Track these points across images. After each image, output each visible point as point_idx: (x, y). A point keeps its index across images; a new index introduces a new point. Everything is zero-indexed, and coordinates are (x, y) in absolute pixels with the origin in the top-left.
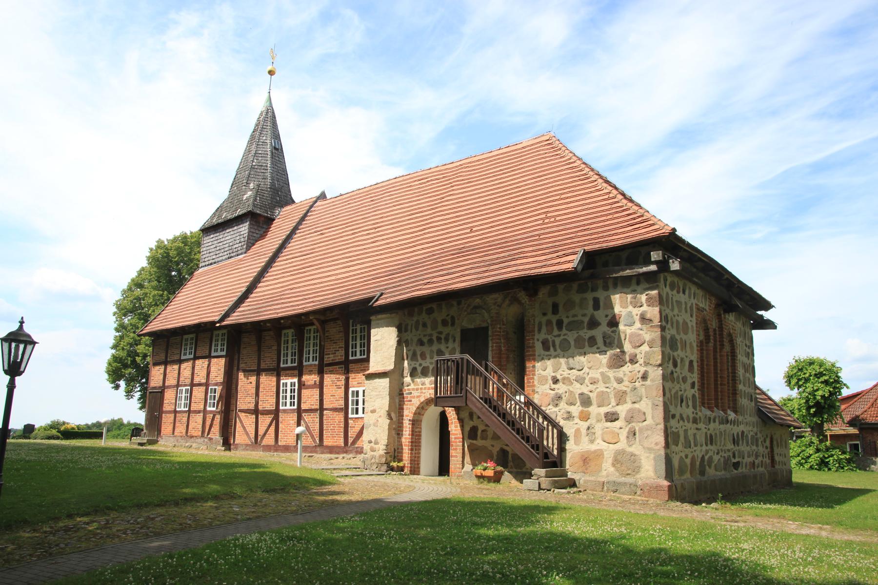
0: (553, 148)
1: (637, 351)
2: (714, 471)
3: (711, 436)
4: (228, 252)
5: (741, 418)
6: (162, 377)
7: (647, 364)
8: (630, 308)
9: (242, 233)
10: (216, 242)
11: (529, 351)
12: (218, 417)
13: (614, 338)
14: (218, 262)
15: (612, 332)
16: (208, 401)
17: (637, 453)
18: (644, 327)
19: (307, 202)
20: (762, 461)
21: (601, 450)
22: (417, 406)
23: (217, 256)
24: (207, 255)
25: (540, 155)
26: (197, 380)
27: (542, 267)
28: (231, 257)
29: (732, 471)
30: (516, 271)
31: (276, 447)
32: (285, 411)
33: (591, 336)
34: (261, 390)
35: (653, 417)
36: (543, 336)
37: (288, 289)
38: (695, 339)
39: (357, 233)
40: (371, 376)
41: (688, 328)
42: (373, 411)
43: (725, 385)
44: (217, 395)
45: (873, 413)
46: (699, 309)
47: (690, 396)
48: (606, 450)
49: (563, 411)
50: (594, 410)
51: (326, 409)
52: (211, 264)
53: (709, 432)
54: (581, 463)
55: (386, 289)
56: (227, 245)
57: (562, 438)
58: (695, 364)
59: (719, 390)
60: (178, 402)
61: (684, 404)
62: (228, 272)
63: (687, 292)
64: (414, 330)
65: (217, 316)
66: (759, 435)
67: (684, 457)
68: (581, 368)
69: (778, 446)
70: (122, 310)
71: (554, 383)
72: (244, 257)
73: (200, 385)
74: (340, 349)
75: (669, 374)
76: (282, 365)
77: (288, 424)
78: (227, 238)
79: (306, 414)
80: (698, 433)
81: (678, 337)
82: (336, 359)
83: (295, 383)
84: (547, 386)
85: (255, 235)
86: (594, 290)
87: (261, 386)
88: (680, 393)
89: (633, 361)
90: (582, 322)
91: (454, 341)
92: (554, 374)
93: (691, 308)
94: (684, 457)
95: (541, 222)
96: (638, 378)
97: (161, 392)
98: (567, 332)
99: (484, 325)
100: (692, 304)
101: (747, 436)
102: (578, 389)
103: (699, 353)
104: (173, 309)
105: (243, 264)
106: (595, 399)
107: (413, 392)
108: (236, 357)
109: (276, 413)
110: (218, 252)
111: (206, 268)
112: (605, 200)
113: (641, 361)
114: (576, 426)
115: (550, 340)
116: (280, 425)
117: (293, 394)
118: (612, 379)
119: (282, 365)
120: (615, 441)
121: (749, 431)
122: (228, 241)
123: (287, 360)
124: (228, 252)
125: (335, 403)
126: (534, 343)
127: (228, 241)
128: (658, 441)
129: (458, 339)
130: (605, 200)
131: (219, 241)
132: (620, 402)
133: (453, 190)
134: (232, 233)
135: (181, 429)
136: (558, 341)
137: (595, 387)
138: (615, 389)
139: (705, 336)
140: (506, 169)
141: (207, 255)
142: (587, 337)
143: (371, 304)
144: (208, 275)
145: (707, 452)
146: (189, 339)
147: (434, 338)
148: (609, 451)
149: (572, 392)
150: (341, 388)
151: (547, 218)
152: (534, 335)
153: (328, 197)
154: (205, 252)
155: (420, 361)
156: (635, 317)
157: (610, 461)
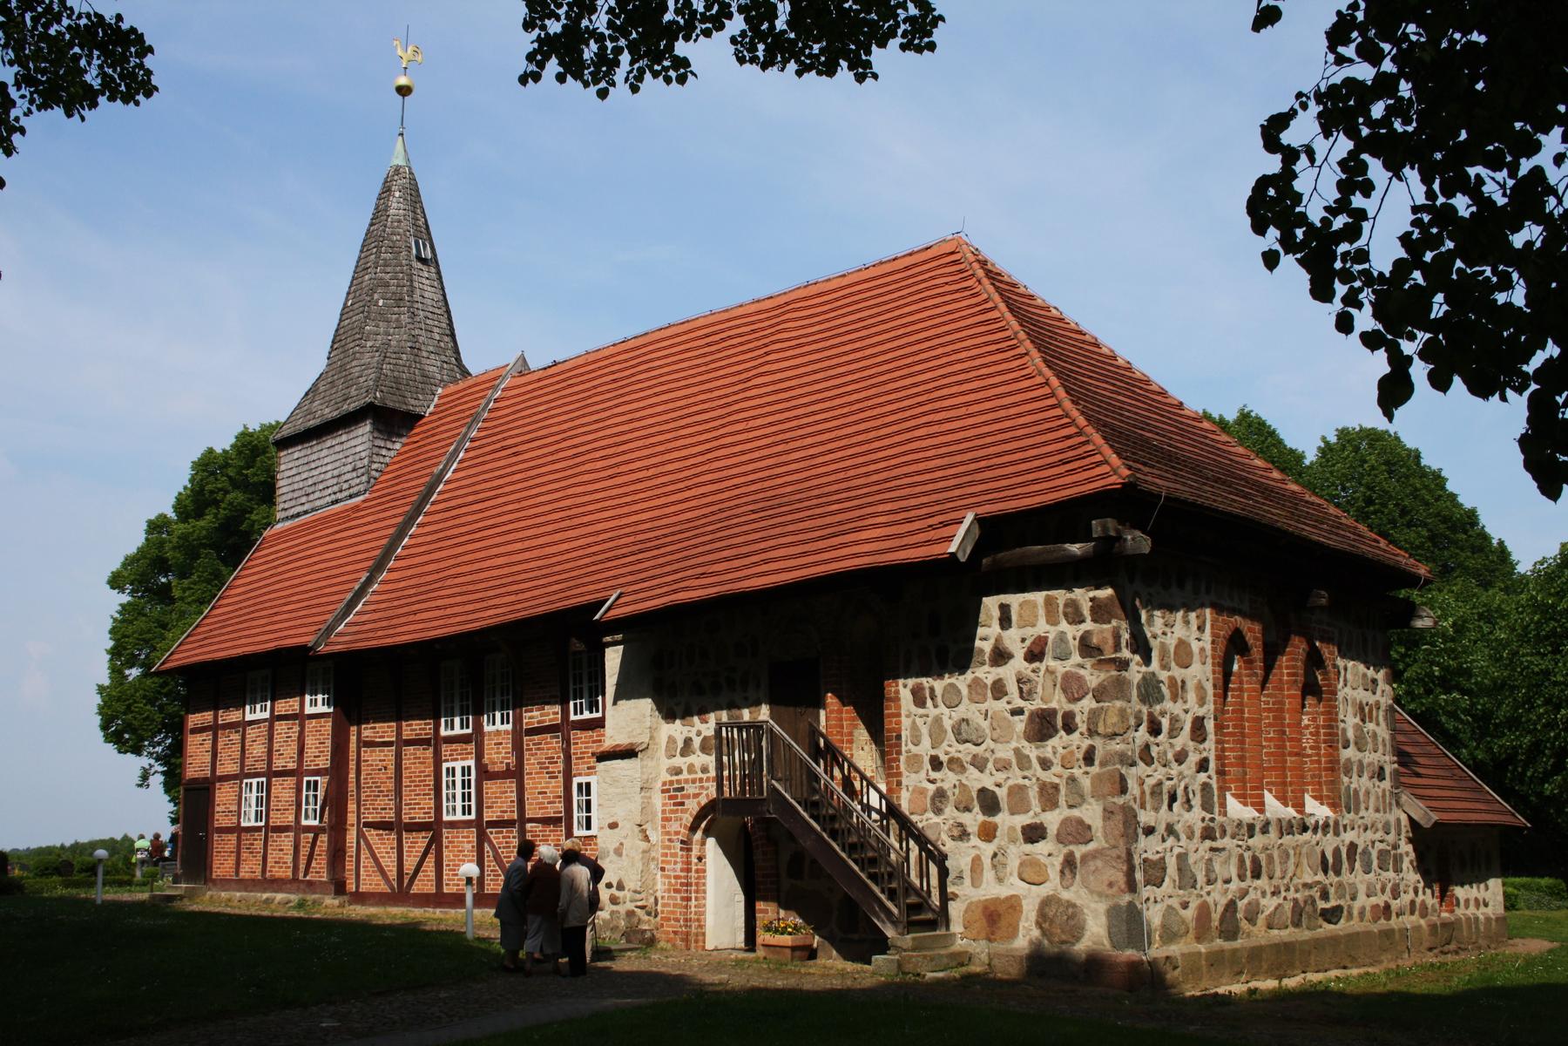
0: (961, 271)
1: (1076, 708)
5: (1348, 818)
6: (208, 758)
7: (1092, 732)
8: (1064, 626)
9: (358, 449)
12: (324, 838)
13: (1037, 683)
15: (1034, 671)
17: (1078, 902)
18: (1088, 662)
20: (1413, 903)
22: (695, 813)
23: (312, 497)
25: (936, 286)
26: (278, 764)
28: (337, 501)
31: (440, 899)
32: (453, 825)
33: (997, 677)
34: (405, 782)
35: (1106, 835)
39: (582, 454)
40: (604, 757)
41: (1190, 654)
42: (613, 826)
44: (320, 793)
47: (1197, 787)
48: (1025, 897)
49: (951, 822)
50: (1003, 820)
53: (1247, 855)
57: (944, 873)
58: (1210, 725)
62: (332, 534)
65: (311, 633)
67: (1177, 906)
68: (980, 741)
71: (933, 770)
72: (364, 501)
77: (461, 851)
79: (494, 830)
81: (1163, 675)
82: (544, 721)
83: (469, 768)
84: (923, 775)
89: (1069, 728)
92: (933, 752)
94: (1177, 906)
96: (1078, 760)
97: (205, 789)
101: (1365, 852)
102: (977, 780)
104: (224, 614)
105: (363, 517)
106: (1005, 799)
107: (686, 786)
109: (434, 828)
111: (288, 524)
113: (1083, 728)
114: (974, 852)
116: (445, 853)
117: (466, 790)
120: (1036, 879)
121: (1373, 843)
125: (547, 808)
126: (897, 692)
128: (1112, 879)
131: (313, 465)
134: (337, 448)
138: (1038, 779)
140: (871, 317)
141: (290, 496)
142: (989, 682)
143: (597, 617)
144: (292, 540)
145: (1244, 894)
149: (964, 785)
150: (557, 777)
153: (533, 365)
157: (1033, 916)
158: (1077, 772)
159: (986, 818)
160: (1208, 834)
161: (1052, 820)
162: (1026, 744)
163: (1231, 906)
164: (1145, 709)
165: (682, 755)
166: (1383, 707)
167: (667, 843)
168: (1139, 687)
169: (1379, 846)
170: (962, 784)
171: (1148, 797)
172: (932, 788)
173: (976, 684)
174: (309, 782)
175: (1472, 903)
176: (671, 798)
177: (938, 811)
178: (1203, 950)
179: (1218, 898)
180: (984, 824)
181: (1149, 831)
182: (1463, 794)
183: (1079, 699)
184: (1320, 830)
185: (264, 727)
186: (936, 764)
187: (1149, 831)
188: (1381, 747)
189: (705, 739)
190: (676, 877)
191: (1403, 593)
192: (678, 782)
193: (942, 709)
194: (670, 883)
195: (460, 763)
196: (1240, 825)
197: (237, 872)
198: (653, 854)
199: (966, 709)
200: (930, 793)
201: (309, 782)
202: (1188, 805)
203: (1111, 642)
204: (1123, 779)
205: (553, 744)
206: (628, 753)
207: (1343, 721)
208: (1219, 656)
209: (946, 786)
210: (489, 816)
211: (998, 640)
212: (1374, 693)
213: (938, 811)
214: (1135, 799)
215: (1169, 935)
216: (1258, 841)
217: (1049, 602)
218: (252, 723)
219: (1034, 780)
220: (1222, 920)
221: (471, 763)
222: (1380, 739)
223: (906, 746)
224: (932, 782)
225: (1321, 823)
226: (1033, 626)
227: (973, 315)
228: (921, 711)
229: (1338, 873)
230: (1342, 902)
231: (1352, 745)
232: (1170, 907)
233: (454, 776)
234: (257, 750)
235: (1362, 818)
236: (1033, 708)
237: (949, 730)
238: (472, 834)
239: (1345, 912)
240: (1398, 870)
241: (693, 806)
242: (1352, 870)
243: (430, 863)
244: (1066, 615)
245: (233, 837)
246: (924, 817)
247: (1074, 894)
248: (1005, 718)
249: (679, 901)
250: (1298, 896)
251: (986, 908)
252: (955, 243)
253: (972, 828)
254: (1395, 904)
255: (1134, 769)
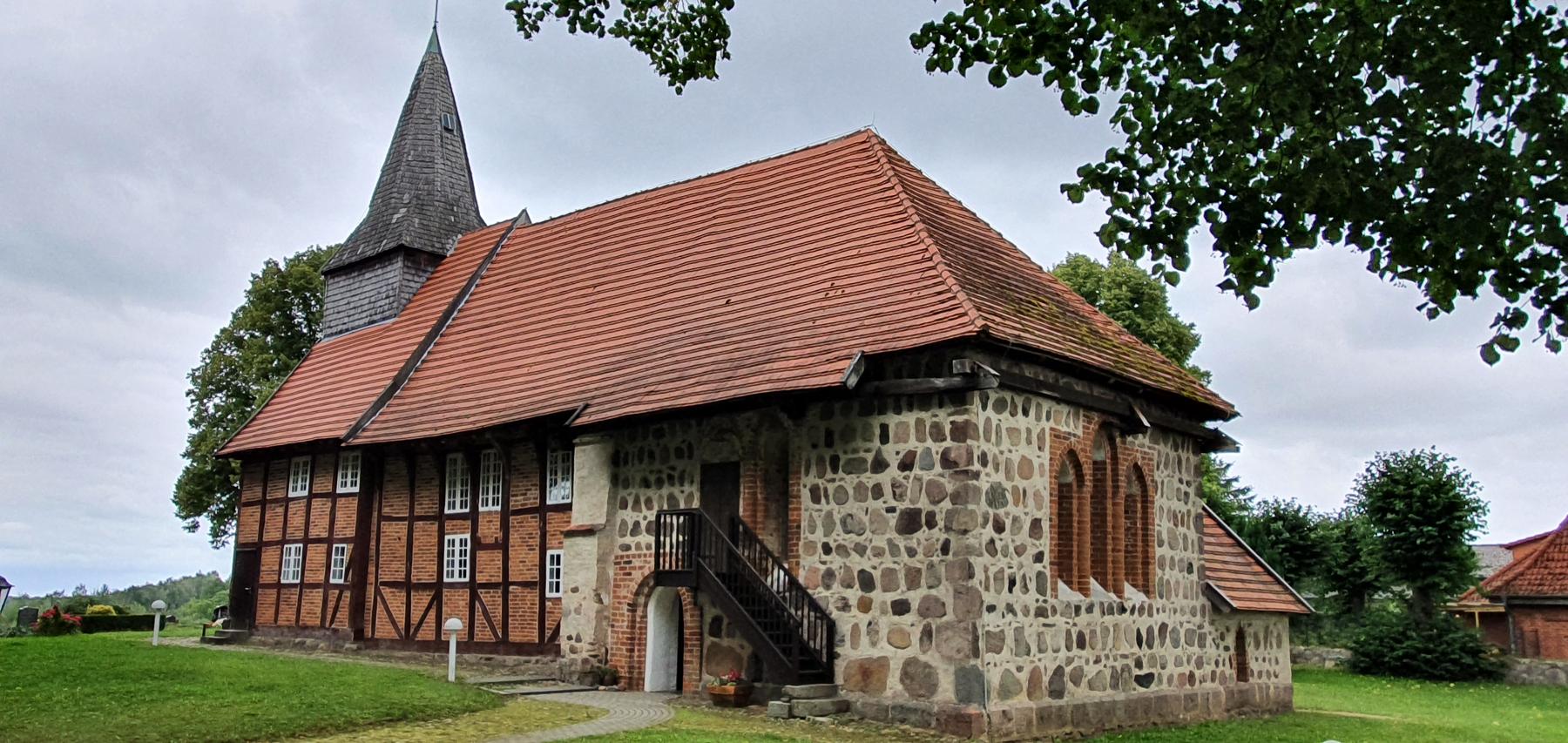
0: (868, 157)
1: (936, 509)
2: (1087, 689)
3: (1081, 636)
4: (368, 313)
5: (1158, 603)
7: (948, 529)
8: (929, 443)
9: (390, 281)
10: (348, 294)
11: (792, 503)
12: (347, 594)
14: (353, 328)
15: (904, 478)
16: (332, 568)
17: (934, 664)
18: (947, 472)
19: (499, 227)
20: (1213, 673)
21: (885, 658)
23: (351, 319)
24: (335, 316)
26: (313, 533)
27: (802, 377)
29: (1135, 689)
30: (769, 381)
32: (452, 585)
36: (810, 480)
37: (458, 387)
38: (1047, 486)
42: (575, 590)
43: (1119, 551)
44: (346, 558)
45: (1533, 577)
46: (1056, 435)
48: (892, 658)
49: (836, 596)
50: (877, 595)
51: (514, 583)
52: (341, 332)
54: (859, 677)
55: (593, 398)
56: (367, 301)
58: (1046, 525)
59: (1110, 559)
60: (283, 569)
61: (1017, 588)
63: (1032, 412)
64: (636, 462)
66: (1207, 628)
67: (1014, 670)
69: (1257, 645)
70: (206, 383)
72: (394, 324)
73: (319, 541)
74: (533, 488)
75: (984, 544)
76: (447, 511)
78: (366, 289)
80: (1049, 632)
81: (1008, 485)
83: (466, 540)
85: (412, 284)
86: (882, 412)
87: (415, 543)
88: (1008, 572)
89: (931, 524)
90: (864, 461)
91: (692, 482)
92: (825, 540)
93: (1041, 438)
94: (1014, 670)
95: (822, 295)
98: (844, 475)
99: (734, 458)
100: (1043, 429)
101: (1174, 630)
102: (857, 563)
103: (1055, 506)
108: (377, 496)
109: (437, 589)
110: (352, 312)
112: (917, 262)
113: (941, 524)
114: (854, 621)
115: (822, 487)
118: (903, 549)
119: (447, 511)
120: (904, 644)
121: (1181, 624)
122: (367, 295)
123: (454, 502)
124: (368, 313)
126: (799, 491)
127: (367, 295)
129: (697, 478)
130: (917, 262)
131: (353, 293)
132: (913, 583)
133: (715, 225)
135: (287, 616)
136: (831, 488)
137: (880, 561)
138: (905, 565)
139: (1077, 475)
141: (335, 316)
142: (870, 485)
145: (1069, 661)
146: (301, 465)
147: (664, 476)
148: (897, 658)
149: (849, 567)
151: (832, 287)
152: (800, 478)
154: (331, 311)
155: (645, 511)
156: (934, 455)
157: (898, 674)
158: (935, 559)
159: (864, 593)
160: (1041, 613)
161: (915, 597)
162: (897, 535)
163: (1059, 671)
164: (991, 511)
165: (632, 535)
166: (1193, 514)
167: (617, 605)
168: (987, 493)
169: (1186, 626)
170: (845, 566)
171: (992, 581)
172: (823, 568)
173: (860, 487)
174: (337, 548)
175: (1264, 674)
176: (622, 569)
177: (828, 587)
178: (1034, 707)
179: (1048, 663)
180: (862, 597)
181: (991, 609)
182: (1261, 587)
183: (939, 502)
184: (1136, 613)
185: (303, 503)
186: (827, 549)
187: (991, 609)
188: (1190, 546)
189: (650, 522)
190: (623, 633)
191: (1210, 425)
192: (628, 556)
193: (833, 504)
194: (618, 638)
195: (458, 538)
196: (1068, 605)
197: (276, 620)
198: (606, 614)
199: (852, 507)
200: (822, 572)
201: (337, 548)
202: (1026, 589)
203: (965, 457)
204: (970, 566)
205: (533, 523)
206: (589, 532)
207: (1159, 525)
208: (1056, 471)
209: (834, 567)
210: (480, 578)
211: (879, 452)
212: (1186, 503)
213: (828, 587)
214: (981, 583)
215: (1006, 692)
216: (1084, 618)
217: (919, 422)
218: (293, 499)
219: (902, 565)
220: (1050, 683)
221: (468, 536)
222: (1190, 542)
223: (805, 535)
224: (824, 563)
225: (1137, 606)
226: (906, 442)
227: (875, 193)
228: (817, 507)
229: (1150, 646)
230: (1153, 670)
231: (1166, 544)
232: (1007, 670)
233: (453, 546)
234: (297, 521)
235: (1173, 603)
236: (903, 507)
237: (838, 522)
238: (466, 594)
239: (1156, 679)
240: (1202, 646)
241: (638, 576)
242: (1162, 644)
243: (415, 619)
244: (931, 435)
245: (274, 591)
246: (816, 591)
247: (931, 657)
248: (881, 515)
249: (625, 652)
250: (1116, 664)
251: (861, 666)
252: (866, 135)
253: (853, 602)
254: (1198, 673)
255: (980, 559)
